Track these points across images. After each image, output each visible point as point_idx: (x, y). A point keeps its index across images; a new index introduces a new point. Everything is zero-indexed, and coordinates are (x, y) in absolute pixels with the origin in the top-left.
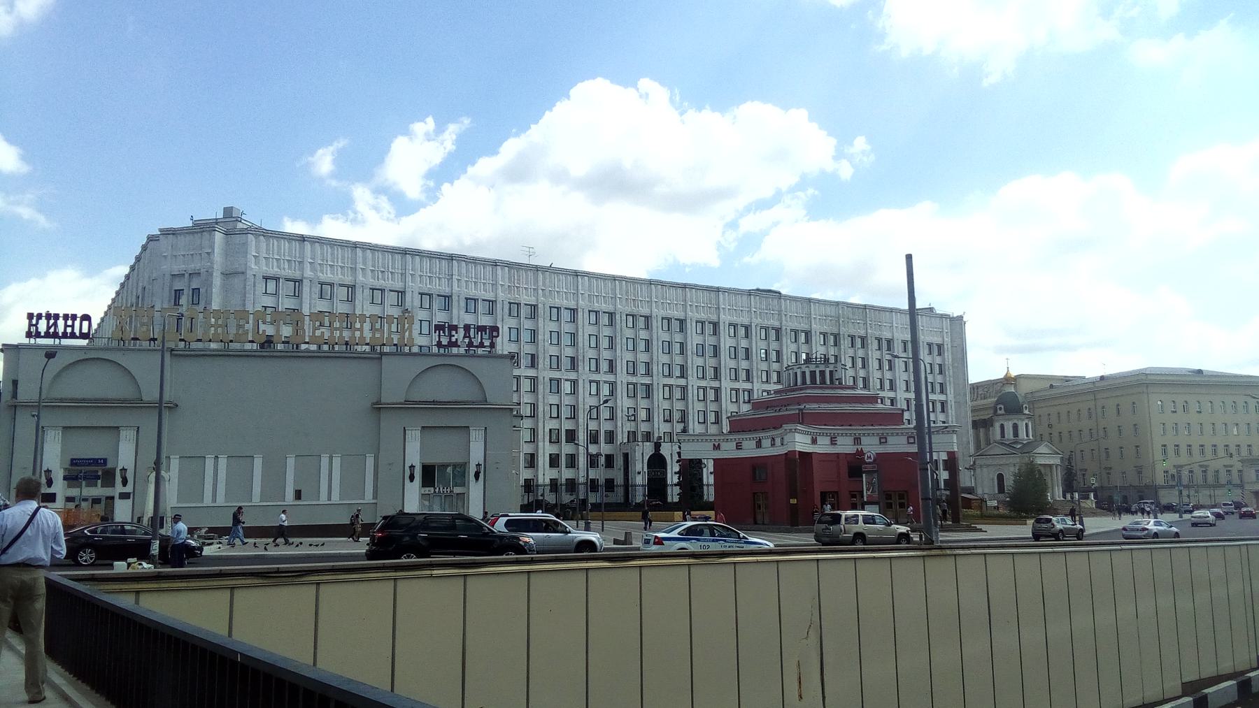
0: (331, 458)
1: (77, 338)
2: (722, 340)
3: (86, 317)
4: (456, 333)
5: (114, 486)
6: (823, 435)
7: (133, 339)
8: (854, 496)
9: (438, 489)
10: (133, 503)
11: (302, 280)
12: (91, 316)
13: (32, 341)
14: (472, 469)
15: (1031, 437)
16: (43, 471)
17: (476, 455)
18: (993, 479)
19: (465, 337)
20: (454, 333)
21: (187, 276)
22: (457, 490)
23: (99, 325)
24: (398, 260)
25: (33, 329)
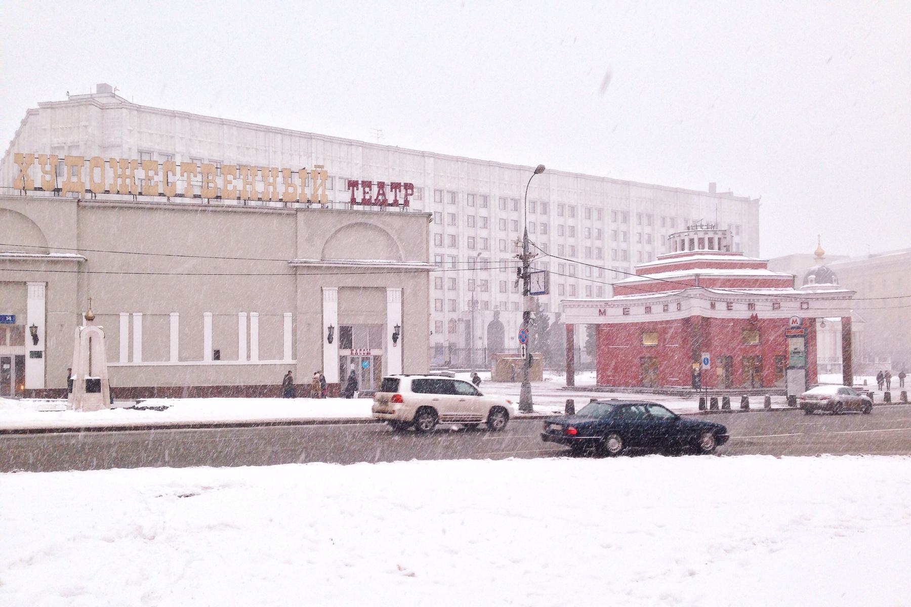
6: (656, 304)
9: (355, 350)
10: (46, 362)
11: (174, 155)
14: (391, 331)
19: (379, 194)
20: (367, 189)
21: (66, 148)
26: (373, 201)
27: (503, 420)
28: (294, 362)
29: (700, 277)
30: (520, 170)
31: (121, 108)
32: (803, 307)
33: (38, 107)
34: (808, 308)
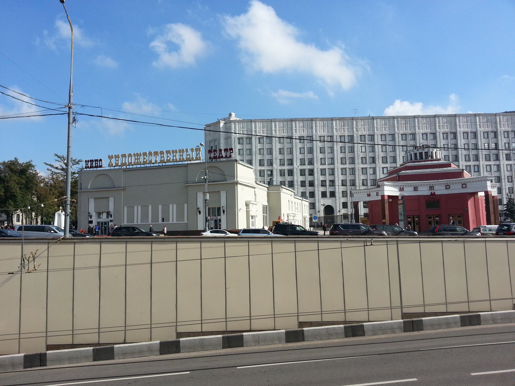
0: (173, 206)
4: (217, 153)
6: (388, 186)
21: (214, 141)
22: (219, 217)
24: (289, 124)
28: (187, 222)
34: (466, 187)
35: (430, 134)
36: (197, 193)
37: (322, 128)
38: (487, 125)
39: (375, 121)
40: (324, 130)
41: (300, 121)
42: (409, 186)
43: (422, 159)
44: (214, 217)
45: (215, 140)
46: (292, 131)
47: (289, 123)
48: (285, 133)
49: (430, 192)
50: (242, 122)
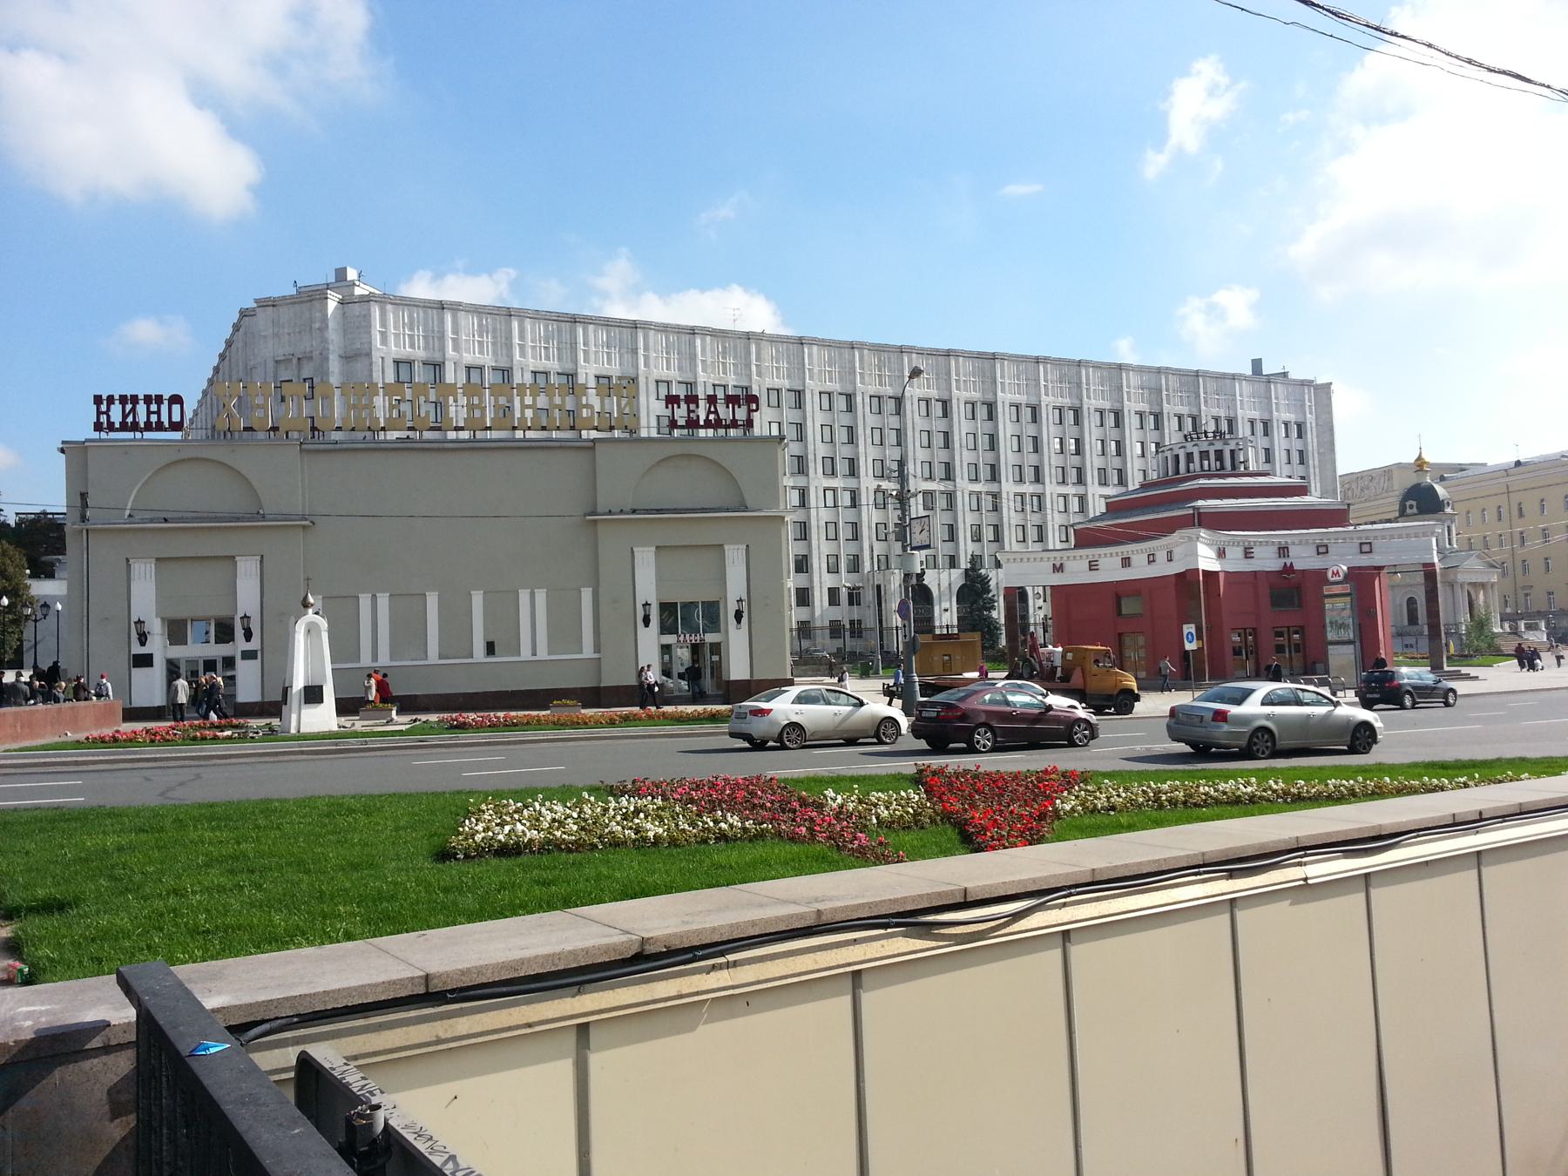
1: (166, 430)
2: (1001, 426)
3: (176, 399)
5: (233, 640)
7: (246, 429)
8: (1280, 634)
12: (181, 395)
13: (104, 435)
14: (732, 607)
15: (1455, 546)
16: (133, 624)
17: (736, 587)
18: (1401, 605)
19: (709, 412)
21: (295, 361)
22: (710, 638)
23: (196, 413)
25: (103, 418)
26: (702, 423)
27: (988, 748)
28: (596, 656)
29: (1201, 511)
30: (949, 356)
31: (368, 301)
32: (1320, 551)
33: (255, 305)
35: (840, 394)
36: (632, 549)
37: (476, 338)
38: (723, 365)
39: (806, 350)
40: (668, 361)
41: (599, 324)
42: (1258, 544)
43: (1222, 468)
44: (693, 638)
45: (299, 359)
46: (574, 355)
47: (566, 327)
48: (554, 360)
49: (1282, 561)
50: (407, 305)
